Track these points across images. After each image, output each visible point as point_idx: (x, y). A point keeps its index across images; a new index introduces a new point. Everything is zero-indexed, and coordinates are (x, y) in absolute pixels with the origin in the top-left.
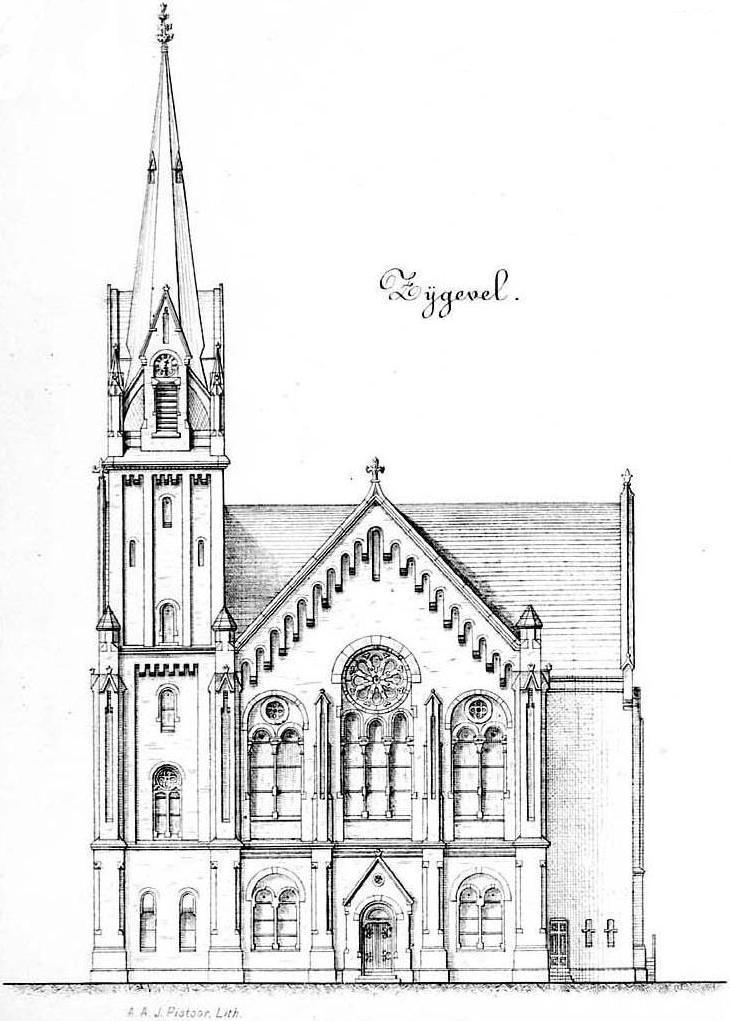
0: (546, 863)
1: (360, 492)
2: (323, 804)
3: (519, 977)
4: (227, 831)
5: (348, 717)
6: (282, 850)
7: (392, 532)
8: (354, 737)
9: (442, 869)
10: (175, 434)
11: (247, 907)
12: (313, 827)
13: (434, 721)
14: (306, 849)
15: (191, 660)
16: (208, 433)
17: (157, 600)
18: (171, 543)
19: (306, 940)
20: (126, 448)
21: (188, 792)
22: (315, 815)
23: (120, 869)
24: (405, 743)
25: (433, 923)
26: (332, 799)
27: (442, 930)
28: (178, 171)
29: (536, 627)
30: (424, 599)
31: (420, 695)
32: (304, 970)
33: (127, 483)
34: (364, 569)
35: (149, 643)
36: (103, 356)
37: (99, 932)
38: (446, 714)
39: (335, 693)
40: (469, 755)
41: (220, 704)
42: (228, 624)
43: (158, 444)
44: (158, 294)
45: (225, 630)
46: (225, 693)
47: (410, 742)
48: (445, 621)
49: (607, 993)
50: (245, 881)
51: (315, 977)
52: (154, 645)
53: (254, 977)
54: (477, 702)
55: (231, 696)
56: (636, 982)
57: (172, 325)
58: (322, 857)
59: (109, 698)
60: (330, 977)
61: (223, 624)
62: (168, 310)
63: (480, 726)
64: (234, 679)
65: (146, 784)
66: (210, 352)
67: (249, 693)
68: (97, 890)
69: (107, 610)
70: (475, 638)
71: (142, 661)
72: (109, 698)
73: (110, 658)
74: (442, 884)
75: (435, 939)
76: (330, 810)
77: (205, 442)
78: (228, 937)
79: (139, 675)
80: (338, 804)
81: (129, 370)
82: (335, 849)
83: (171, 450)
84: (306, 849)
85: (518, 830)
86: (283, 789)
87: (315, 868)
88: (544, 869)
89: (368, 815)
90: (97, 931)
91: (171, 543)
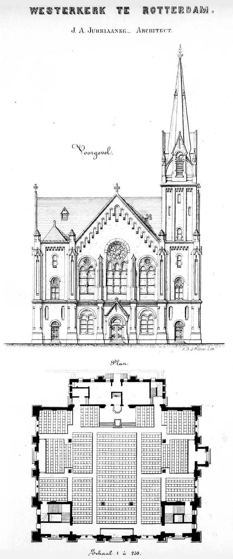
0: (42, 307)
1: (113, 193)
2: (100, 288)
3: (158, 342)
4: (73, 298)
5: (108, 263)
6: (89, 303)
7: (122, 205)
8: (110, 269)
9: (136, 309)
10: (182, 176)
11: (138, 320)
12: (97, 297)
13: (134, 264)
14: (96, 304)
15: (186, 245)
16: (192, 176)
17: (176, 227)
18: (180, 208)
19: (95, 331)
20: (166, 181)
21: (61, 285)
22: (131, 293)
23: (135, 309)
24: (93, 271)
25: (133, 326)
26: (137, 287)
27: (136, 328)
28: (183, 94)
29: (198, 236)
30: (131, 226)
31: (130, 256)
32: (69, 340)
33: (167, 191)
34: (113, 218)
35: (173, 240)
36: (161, 153)
37: (193, 328)
38: (137, 262)
39: (104, 256)
40: (84, 274)
41: (71, 259)
42: (73, 234)
43: (177, 179)
44: (178, 134)
45: (37, 236)
46: (38, 256)
47: (126, 271)
48: (137, 232)
49: (83, 347)
50: (138, 312)
51: (98, 342)
52: (175, 241)
53: (81, 342)
54: (147, 259)
55: (39, 257)
56: (137, 344)
57: (181, 142)
58: (100, 305)
59: (196, 257)
60: (166, 342)
61: (37, 234)
62: (181, 139)
63: (147, 266)
64: (75, 252)
65: (49, 284)
66: (192, 151)
67: (79, 257)
68: (34, 315)
69: (196, 230)
70: (145, 237)
71: (48, 245)
72: (196, 257)
73: (38, 244)
74: (76, 314)
75: (133, 331)
76: (136, 291)
77: (191, 179)
78: (73, 330)
79: (47, 249)
80: (138, 289)
81: (168, 157)
82: (104, 304)
83: (180, 180)
84: (96, 304)
85: (131, 297)
86: (89, 285)
87: (69, 309)
88: (165, 310)
89: (148, 293)
90: (34, 328)
91: (180, 208)
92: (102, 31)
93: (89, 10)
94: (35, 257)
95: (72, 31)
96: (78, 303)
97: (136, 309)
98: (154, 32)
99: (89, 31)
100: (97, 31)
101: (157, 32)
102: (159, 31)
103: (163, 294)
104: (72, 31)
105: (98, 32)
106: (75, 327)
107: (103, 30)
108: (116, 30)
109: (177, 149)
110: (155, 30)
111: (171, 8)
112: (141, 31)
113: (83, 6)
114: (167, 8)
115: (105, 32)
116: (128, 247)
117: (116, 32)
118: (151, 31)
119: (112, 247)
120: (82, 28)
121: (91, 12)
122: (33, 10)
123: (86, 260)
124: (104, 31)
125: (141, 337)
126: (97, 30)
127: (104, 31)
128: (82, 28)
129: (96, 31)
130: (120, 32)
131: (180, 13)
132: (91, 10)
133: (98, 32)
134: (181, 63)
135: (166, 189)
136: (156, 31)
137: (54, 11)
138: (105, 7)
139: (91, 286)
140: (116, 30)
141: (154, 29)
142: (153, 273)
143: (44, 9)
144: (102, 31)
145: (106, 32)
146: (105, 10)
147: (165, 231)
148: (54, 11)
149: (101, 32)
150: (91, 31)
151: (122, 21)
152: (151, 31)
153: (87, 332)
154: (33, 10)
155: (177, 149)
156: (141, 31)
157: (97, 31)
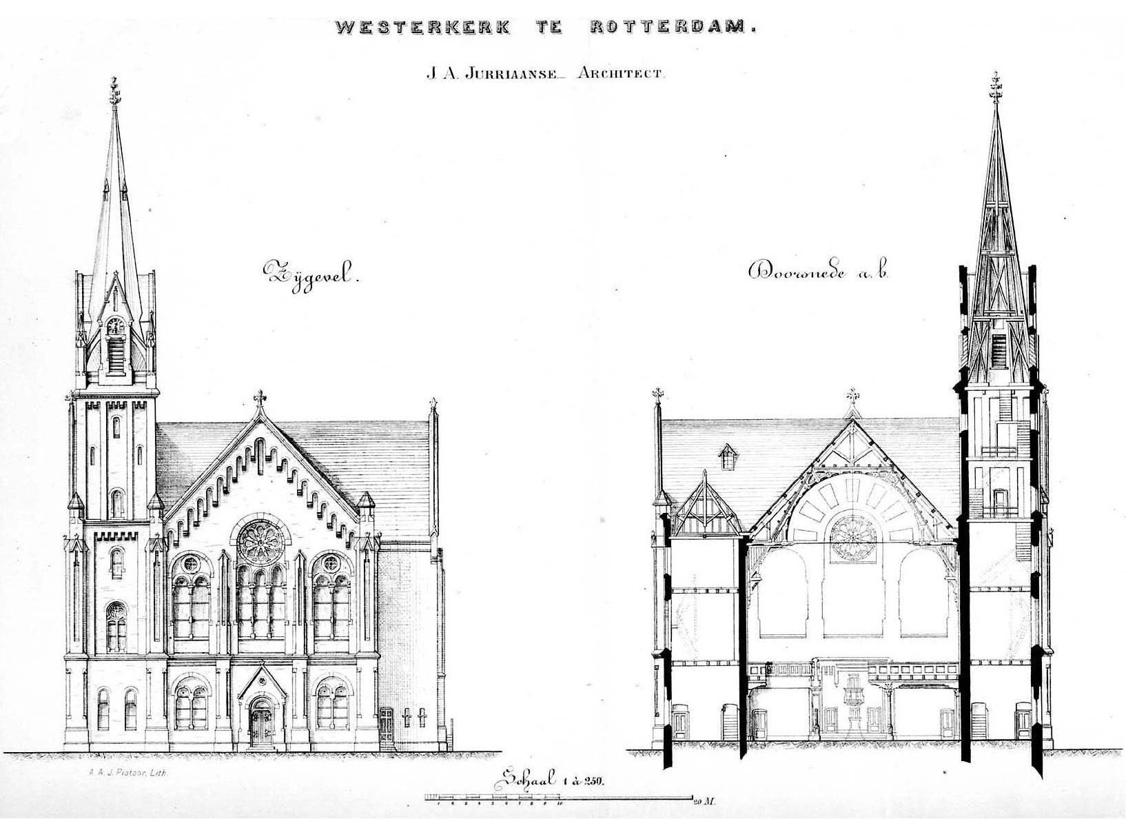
0: (378, 669)
1: (249, 413)
2: (224, 629)
4: (158, 647)
5: (241, 569)
6: (196, 660)
7: (271, 441)
8: (246, 582)
9: (306, 674)
10: (122, 374)
11: (172, 700)
12: (216, 644)
13: (301, 572)
14: (212, 660)
15: (133, 529)
16: (145, 373)
19: (212, 723)
20: (88, 383)
22: (218, 637)
26: (230, 625)
27: (306, 716)
30: (294, 488)
31: (291, 553)
32: (211, 743)
34: (252, 467)
35: (104, 518)
36: (72, 320)
38: (309, 566)
39: (232, 552)
41: (153, 560)
43: (111, 380)
44: (111, 277)
45: (156, 509)
46: (157, 552)
47: (284, 586)
50: (170, 682)
51: (218, 748)
52: (108, 519)
53: (176, 748)
54: (330, 559)
55: (161, 554)
56: (439, 752)
57: (120, 298)
58: (224, 665)
59: (76, 556)
60: (229, 748)
61: (155, 505)
62: (117, 288)
63: (332, 575)
66: (146, 317)
67: (173, 552)
68: (68, 688)
72: (76, 556)
73: (77, 528)
74: (306, 684)
76: (229, 633)
77: (143, 379)
79: (97, 539)
80: (235, 629)
81: (91, 329)
82: (232, 660)
83: (119, 384)
84: (212, 660)
86: (196, 618)
87: (219, 673)
90: (68, 716)
92: (499, 75)
93: (472, 27)
94: (71, 554)
95: (467, 76)
96: (232, 659)
97: (306, 674)
98: (621, 77)
99: (469, 76)
100: (488, 75)
101: (629, 76)
102: (632, 75)
103: (162, 640)
104: (467, 76)
105: (489, 76)
106: (1048, 711)
107: (492, 72)
108: (531, 72)
109: (109, 312)
110: (623, 72)
111: (549, 23)
112: (590, 75)
113: (463, 17)
114: (647, 24)
115: (508, 78)
116: (286, 535)
117: (532, 76)
118: (614, 76)
119: (248, 533)
120: (584, 67)
121: (477, 30)
122: (345, 27)
123: (190, 561)
124: (505, 75)
125: (177, 736)
126: (487, 72)
127: (505, 75)
128: (450, 68)
129: (485, 73)
130: (540, 77)
131: (449, 32)
132: (476, 27)
133: (489, 76)
134: (118, 127)
135: (87, 403)
136: (625, 75)
137: (393, 29)
138: (508, 22)
139: (200, 620)
140: (531, 72)
141: (621, 72)
142: (205, 591)
143: (421, 23)
144: (499, 75)
145: (510, 76)
146: (508, 27)
147: (83, 499)
148: (393, 29)
149: (487, 78)
150: (473, 73)
151: (544, 53)
152: (614, 76)
153: (332, 726)
154: (345, 27)
155: (109, 312)
156: (590, 75)
157: (488, 75)
